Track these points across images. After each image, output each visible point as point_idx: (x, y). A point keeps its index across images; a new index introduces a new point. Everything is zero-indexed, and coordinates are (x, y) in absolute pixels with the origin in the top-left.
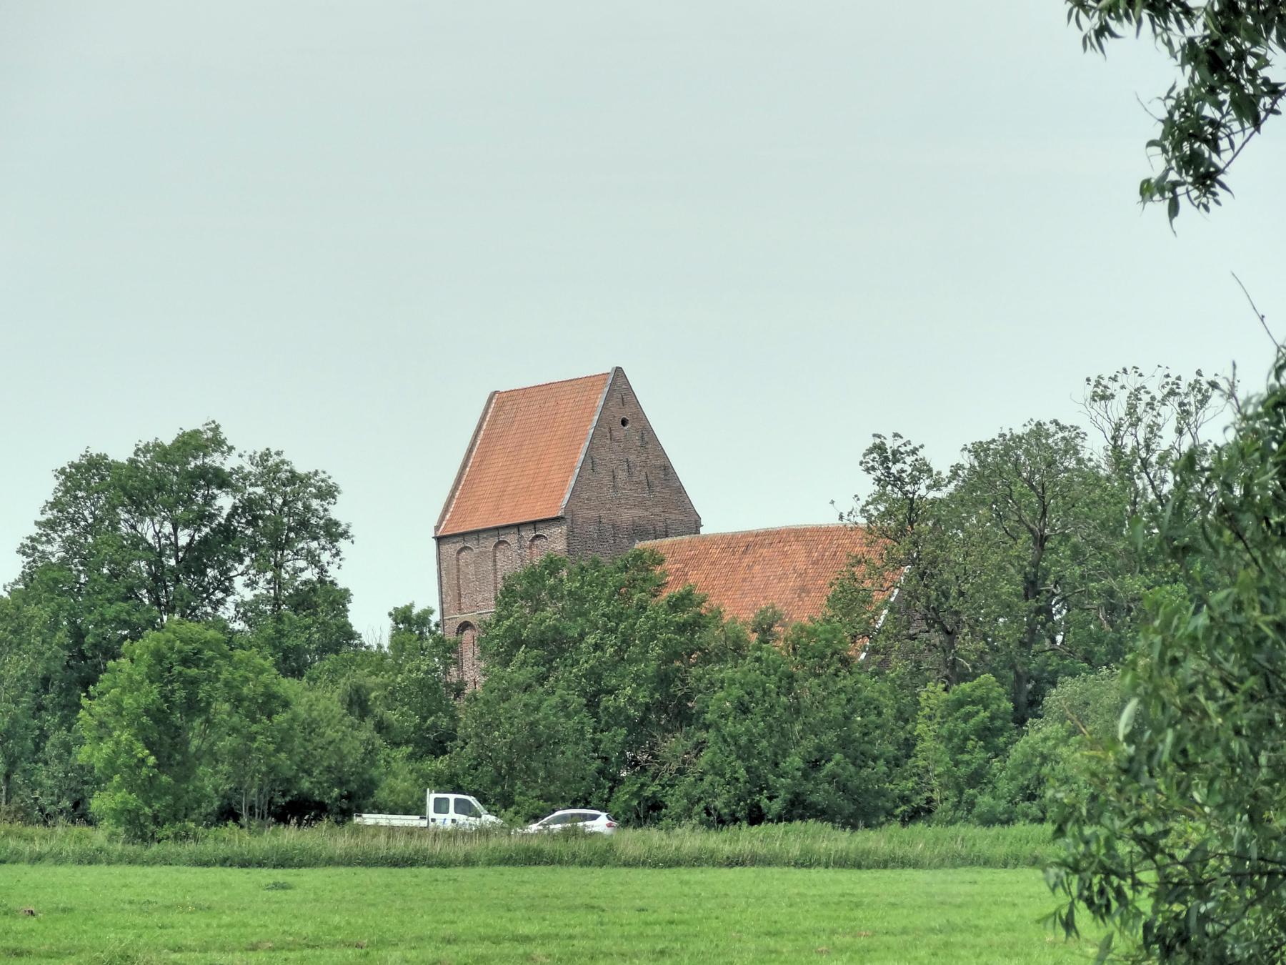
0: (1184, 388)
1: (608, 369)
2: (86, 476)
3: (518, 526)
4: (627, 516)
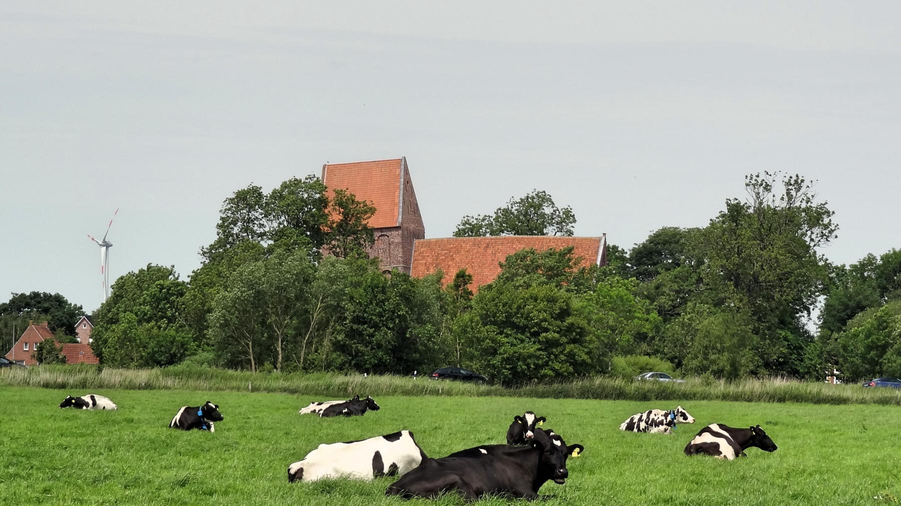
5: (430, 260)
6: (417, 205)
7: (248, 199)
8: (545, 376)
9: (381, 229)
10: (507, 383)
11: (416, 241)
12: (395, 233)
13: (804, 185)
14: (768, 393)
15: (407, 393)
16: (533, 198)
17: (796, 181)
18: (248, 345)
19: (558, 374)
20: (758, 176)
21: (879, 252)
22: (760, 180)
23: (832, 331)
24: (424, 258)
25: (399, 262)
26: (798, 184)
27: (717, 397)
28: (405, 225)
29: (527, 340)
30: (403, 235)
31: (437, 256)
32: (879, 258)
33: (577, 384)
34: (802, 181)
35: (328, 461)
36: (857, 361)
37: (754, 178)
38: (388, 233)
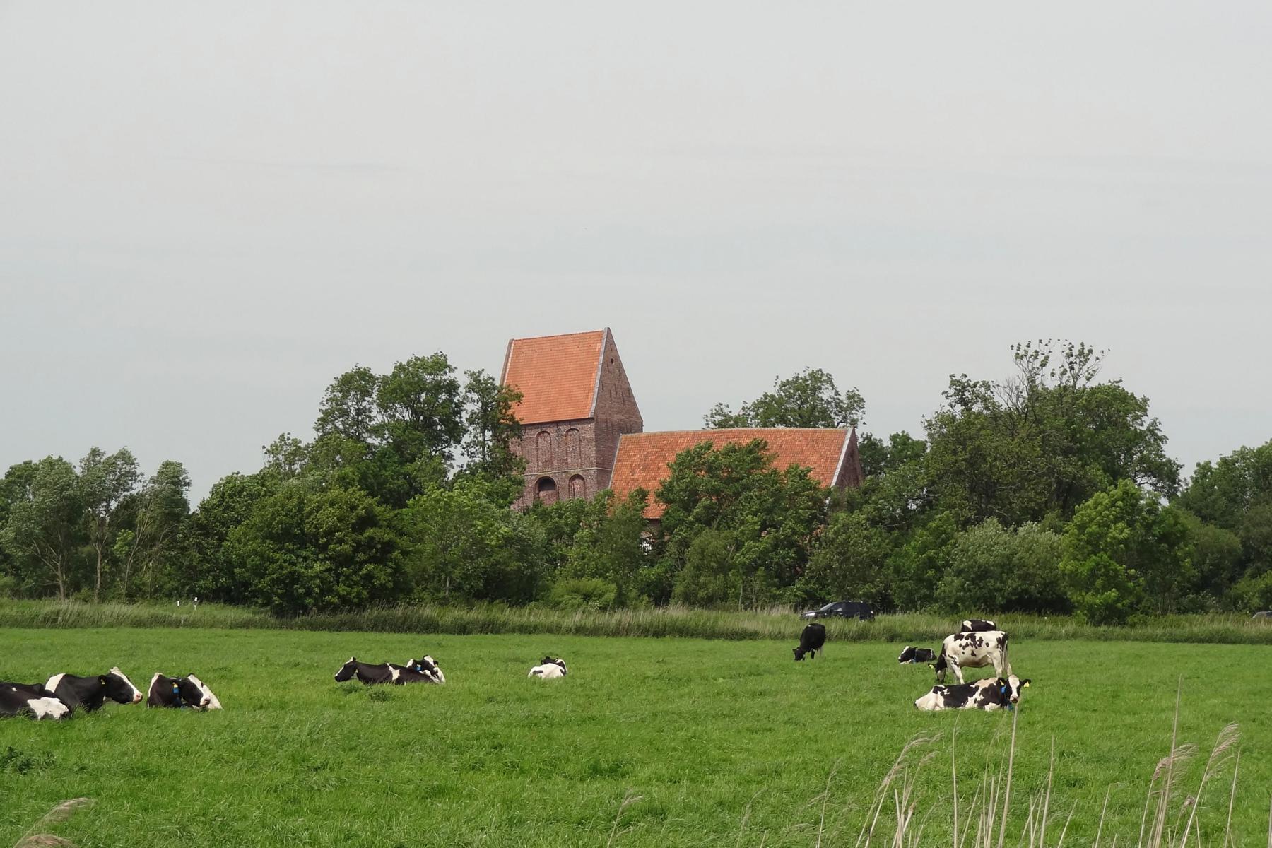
0: (1075, 352)
1: (601, 327)
2: (355, 383)
3: (557, 423)
4: (617, 418)
5: (637, 461)
6: (629, 390)
7: (356, 383)
8: (329, 603)
9: (570, 422)
10: (279, 612)
11: (622, 437)
12: (587, 426)
13: (1092, 357)
14: (639, 626)
15: (138, 623)
16: (805, 380)
17: (1081, 353)
18: (55, 565)
19: (345, 600)
20: (1028, 346)
21: (1255, 444)
22: (1031, 351)
23: (547, 547)
24: (629, 458)
25: (591, 464)
26: (1084, 355)
27: (568, 631)
28: (601, 416)
29: (312, 557)
30: (596, 429)
31: (646, 456)
32: (77, 464)
33: (371, 613)
34: (1090, 351)
35: (215, 703)
36: (910, 585)
37: (1023, 347)
38: (579, 427)
